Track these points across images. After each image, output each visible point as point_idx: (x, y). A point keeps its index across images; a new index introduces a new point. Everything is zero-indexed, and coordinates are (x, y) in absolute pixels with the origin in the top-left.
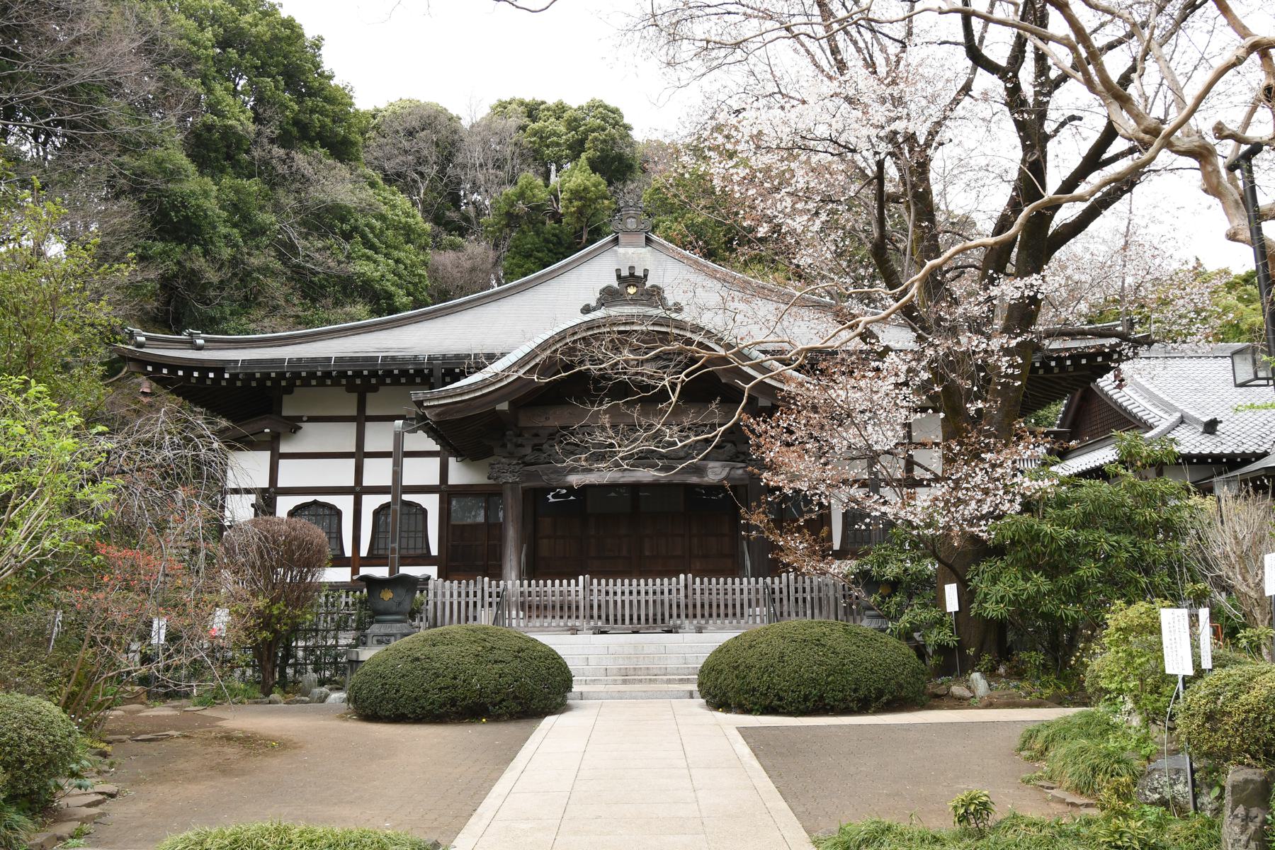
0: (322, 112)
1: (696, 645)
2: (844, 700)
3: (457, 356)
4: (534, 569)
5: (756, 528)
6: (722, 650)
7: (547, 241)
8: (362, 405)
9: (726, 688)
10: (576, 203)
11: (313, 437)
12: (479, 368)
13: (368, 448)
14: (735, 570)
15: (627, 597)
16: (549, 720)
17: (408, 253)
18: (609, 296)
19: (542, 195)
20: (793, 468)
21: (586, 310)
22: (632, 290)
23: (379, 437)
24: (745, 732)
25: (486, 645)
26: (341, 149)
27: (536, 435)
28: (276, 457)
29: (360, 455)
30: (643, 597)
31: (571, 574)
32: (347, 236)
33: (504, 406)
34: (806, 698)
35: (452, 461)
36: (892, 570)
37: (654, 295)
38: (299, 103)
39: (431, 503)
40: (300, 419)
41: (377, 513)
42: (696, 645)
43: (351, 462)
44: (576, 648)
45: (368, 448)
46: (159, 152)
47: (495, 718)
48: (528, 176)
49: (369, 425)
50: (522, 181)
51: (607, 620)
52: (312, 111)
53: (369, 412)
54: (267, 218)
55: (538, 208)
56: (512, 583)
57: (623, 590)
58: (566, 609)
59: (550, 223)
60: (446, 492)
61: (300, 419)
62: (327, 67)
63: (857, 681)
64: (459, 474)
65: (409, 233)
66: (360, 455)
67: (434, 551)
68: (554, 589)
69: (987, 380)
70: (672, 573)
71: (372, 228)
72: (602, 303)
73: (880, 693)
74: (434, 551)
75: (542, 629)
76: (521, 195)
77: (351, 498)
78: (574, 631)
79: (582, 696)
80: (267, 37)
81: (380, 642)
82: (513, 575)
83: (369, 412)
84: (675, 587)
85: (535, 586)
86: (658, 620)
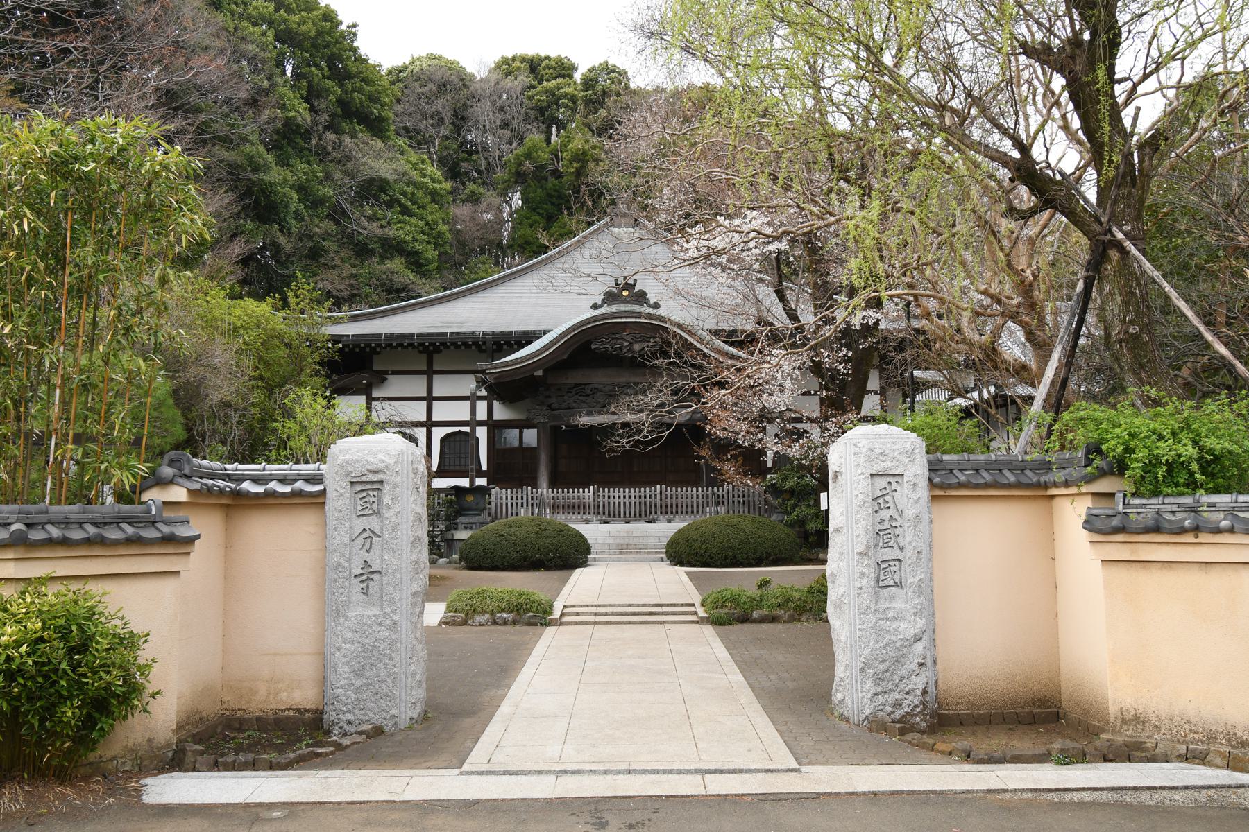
0: (360, 91)
1: (664, 530)
2: (748, 558)
3: (502, 333)
4: (554, 483)
5: (704, 458)
6: (681, 531)
7: (550, 196)
8: (430, 363)
9: (679, 553)
10: (575, 165)
11: (396, 386)
12: (521, 346)
13: (435, 394)
14: (696, 483)
15: (622, 500)
16: (578, 570)
17: (432, 213)
18: (610, 298)
19: (544, 156)
20: (727, 422)
21: (595, 307)
22: (625, 293)
23: (442, 386)
24: (688, 574)
25: (542, 529)
26: (377, 127)
27: (559, 389)
28: (370, 400)
29: (430, 399)
30: (617, 501)
31: (585, 484)
32: (389, 205)
33: (539, 373)
34: (726, 558)
35: (496, 404)
36: (789, 484)
37: (641, 297)
38: (341, 85)
39: (482, 433)
40: (386, 372)
41: (443, 440)
42: (664, 530)
43: (424, 403)
44: (592, 531)
45: (435, 394)
46: (248, 148)
47: (548, 568)
48: (534, 137)
49: (436, 377)
50: (528, 142)
51: (608, 515)
52: (354, 90)
53: (436, 368)
54: (327, 191)
55: (541, 168)
56: (544, 490)
57: (620, 495)
58: (582, 508)
59: (552, 181)
60: (495, 427)
61: (386, 372)
62: (362, 51)
63: (755, 548)
64: (501, 413)
65: (434, 196)
66: (430, 399)
67: (484, 467)
68: (574, 494)
69: (832, 377)
70: (651, 483)
71: (404, 194)
72: (604, 302)
73: (769, 555)
74: (484, 467)
75: (577, 521)
76: (528, 156)
77: (434, 429)
78: (587, 521)
79: (595, 560)
80: (313, 34)
81: (466, 528)
82: (545, 485)
83: (436, 368)
84: (654, 493)
85: (559, 493)
86: (644, 514)
